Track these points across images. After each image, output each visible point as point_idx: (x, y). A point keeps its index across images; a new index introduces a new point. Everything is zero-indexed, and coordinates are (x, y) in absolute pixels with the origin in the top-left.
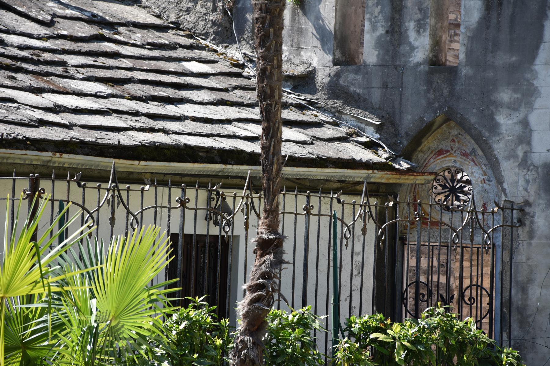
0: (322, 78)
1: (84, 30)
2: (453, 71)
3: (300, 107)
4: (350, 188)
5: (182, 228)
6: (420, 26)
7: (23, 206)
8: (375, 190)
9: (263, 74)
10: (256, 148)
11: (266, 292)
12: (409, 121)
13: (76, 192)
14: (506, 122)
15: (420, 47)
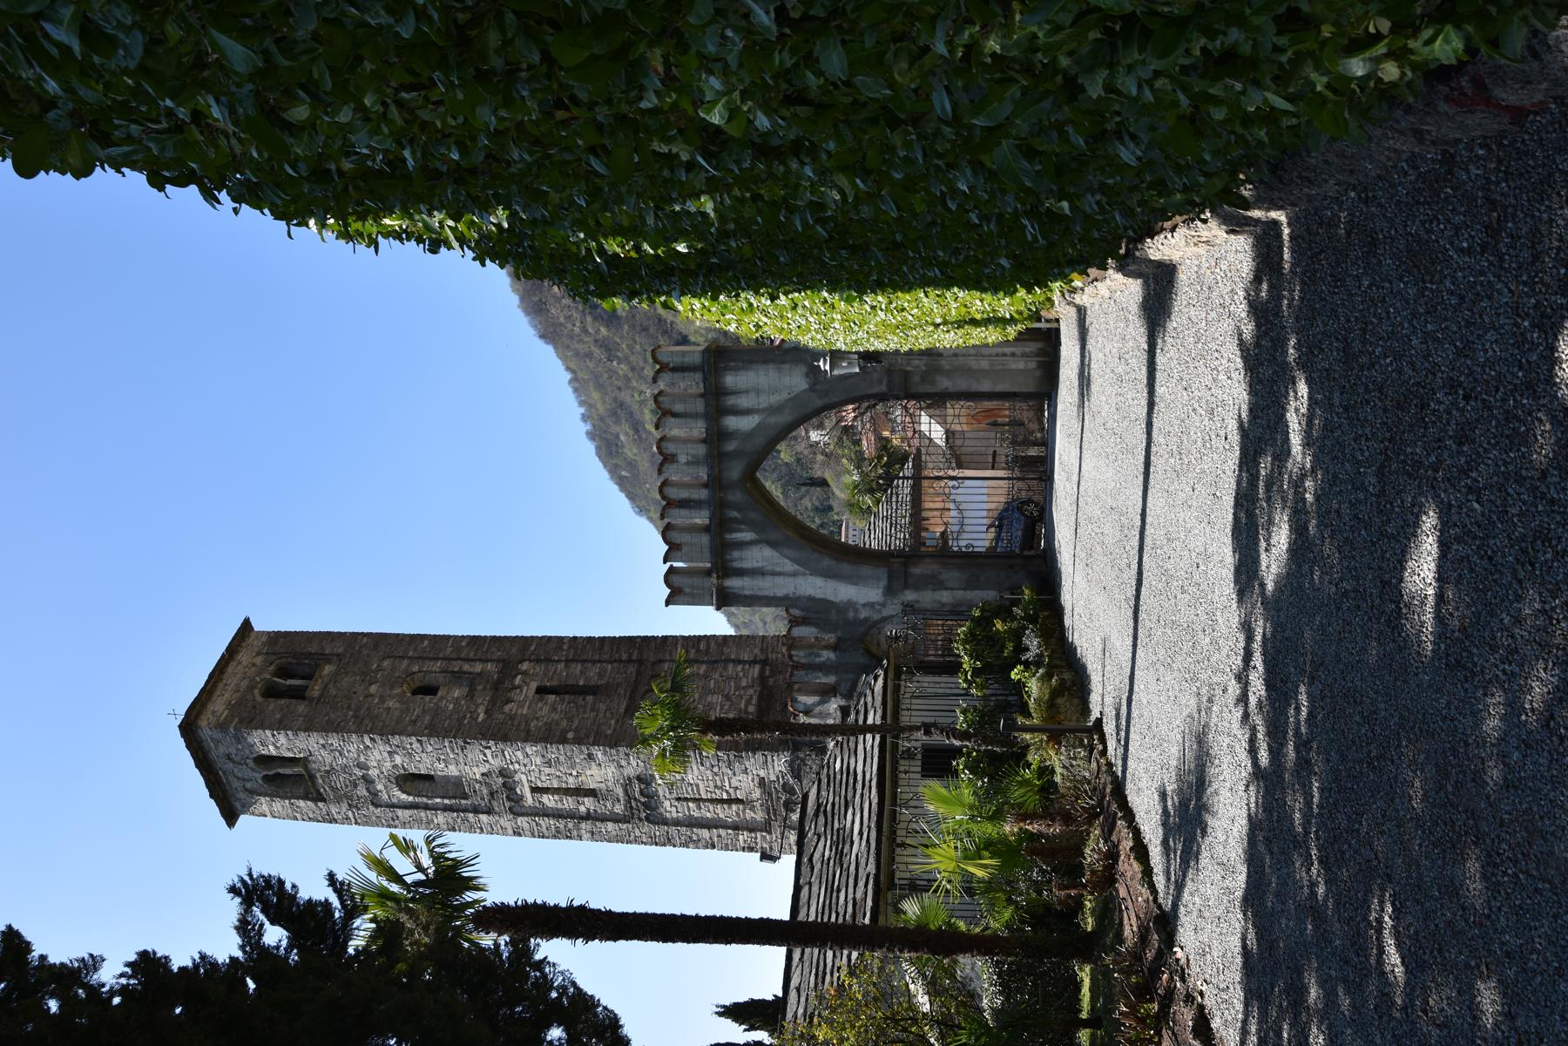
1: (821, 819)
2: (839, 639)
3: (857, 713)
4: (897, 689)
5: (803, 953)
6: (818, 655)
7: (910, 851)
8: (898, 676)
10: (878, 737)
11: (951, 731)
12: (862, 660)
13: (903, 825)
14: (863, 614)
15: (827, 655)
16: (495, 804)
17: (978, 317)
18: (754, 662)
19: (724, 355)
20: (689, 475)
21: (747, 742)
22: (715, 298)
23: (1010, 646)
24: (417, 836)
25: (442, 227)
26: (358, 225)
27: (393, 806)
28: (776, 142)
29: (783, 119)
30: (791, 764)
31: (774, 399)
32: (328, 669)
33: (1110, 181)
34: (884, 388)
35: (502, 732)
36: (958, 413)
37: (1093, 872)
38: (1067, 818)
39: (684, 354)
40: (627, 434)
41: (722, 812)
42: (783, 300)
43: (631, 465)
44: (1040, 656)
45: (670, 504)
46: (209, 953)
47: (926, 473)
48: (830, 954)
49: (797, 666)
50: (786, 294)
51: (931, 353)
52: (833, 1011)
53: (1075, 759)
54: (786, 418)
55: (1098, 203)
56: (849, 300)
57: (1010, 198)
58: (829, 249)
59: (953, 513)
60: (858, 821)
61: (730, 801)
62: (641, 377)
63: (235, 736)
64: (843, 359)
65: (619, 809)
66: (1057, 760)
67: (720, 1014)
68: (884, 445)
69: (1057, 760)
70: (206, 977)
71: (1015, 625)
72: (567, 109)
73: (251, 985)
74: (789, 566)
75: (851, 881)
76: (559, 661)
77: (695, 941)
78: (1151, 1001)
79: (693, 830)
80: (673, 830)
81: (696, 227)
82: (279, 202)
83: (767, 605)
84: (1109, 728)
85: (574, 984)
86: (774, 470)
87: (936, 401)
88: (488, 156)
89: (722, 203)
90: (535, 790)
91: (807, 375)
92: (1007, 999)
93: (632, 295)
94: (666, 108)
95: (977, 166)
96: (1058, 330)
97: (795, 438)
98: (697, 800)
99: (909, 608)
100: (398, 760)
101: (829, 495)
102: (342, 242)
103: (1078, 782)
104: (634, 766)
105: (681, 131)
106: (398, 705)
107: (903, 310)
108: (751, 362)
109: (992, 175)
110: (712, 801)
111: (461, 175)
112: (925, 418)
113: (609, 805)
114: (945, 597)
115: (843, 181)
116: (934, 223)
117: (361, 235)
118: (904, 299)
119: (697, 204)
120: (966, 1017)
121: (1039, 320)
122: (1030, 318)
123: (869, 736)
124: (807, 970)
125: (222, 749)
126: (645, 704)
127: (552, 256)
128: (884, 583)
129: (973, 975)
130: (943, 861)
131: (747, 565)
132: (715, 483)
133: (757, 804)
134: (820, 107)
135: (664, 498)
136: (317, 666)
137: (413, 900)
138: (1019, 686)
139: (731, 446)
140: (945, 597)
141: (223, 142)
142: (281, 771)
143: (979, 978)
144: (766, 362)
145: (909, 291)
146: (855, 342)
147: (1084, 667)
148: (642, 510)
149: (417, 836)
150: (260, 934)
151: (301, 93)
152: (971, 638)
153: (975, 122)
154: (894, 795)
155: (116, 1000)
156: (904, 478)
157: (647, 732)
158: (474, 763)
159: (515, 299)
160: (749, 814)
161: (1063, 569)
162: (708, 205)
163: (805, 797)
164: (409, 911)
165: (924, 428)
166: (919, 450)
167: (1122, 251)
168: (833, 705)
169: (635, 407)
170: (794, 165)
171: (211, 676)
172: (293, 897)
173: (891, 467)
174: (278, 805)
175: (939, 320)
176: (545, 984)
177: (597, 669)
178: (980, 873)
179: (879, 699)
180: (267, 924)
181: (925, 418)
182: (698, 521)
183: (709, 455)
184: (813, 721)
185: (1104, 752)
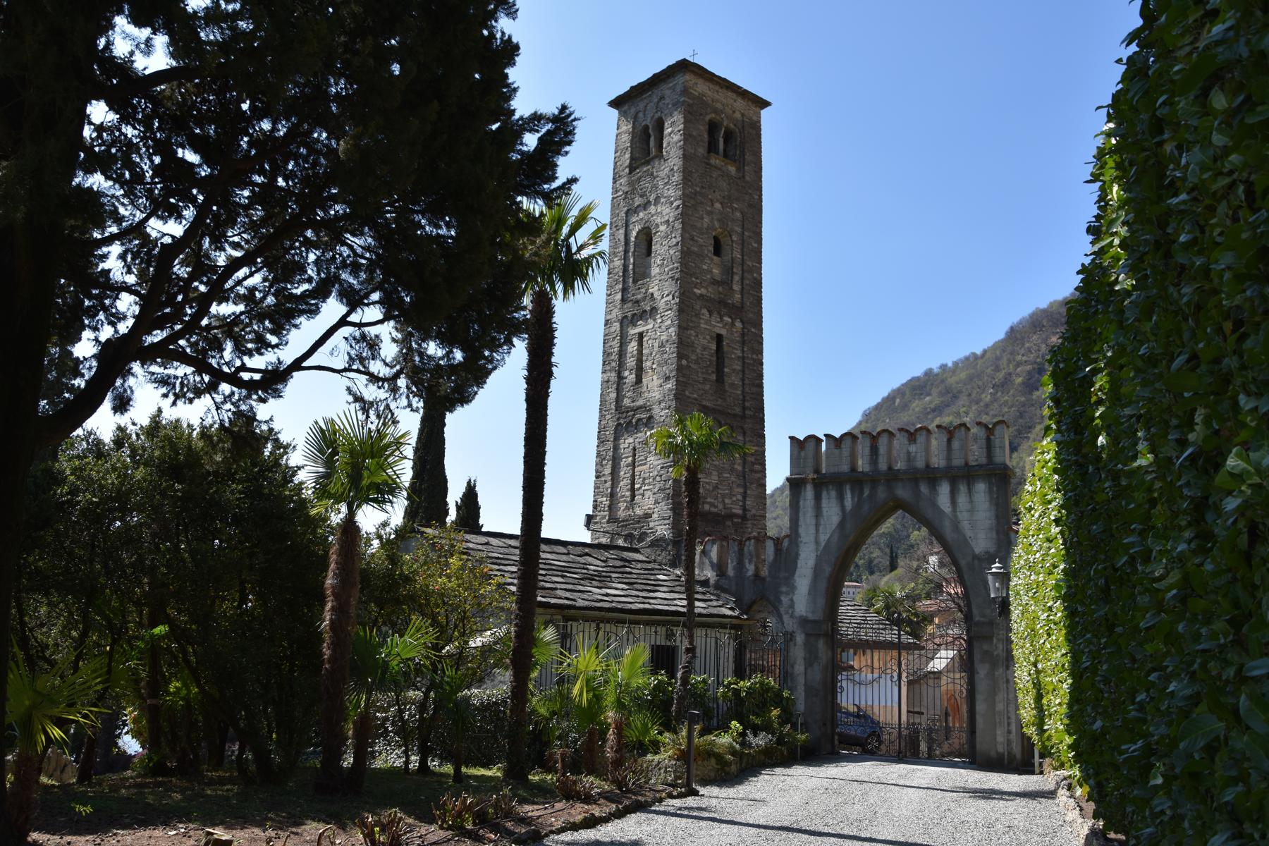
0: (712, 582)
1: (618, 563)
2: (764, 579)
4: (724, 626)
7: (593, 634)
8: (734, 627)
9: (687, 581)
10: (684, 610)
11: (688, 670)
13: (614, 629)
14: (784, 599)
15: (750, 569)
16: (630, 305)
17: (1044, 701)
18: (745, 509)
19: (1003, 482)
20: (898, 454)
21: (681, 504)
22: (1055, 471)
23: (758, 721)
24: (604, 245)
25: (1113, 234)
26: (1111, 164)
27: (627, 226)
28: (1209, 517)
29: (1235, 522)
30: (663, 539)
31: (965, 525)
32: (732, 169)
33: (1186, 825)
34: (977, 619)
35: (686, 309)
36: (956, 684)
37: (575, 782)
38: (618, 763)
39: (1002, 448)
40: (931, 402)
41: (624, 483)
42: (1055, 530)
43: (905, 407)
44: (750, 747)
45: (874, 439)
46: (518, 94)
47: (904, 654)
48: (514, 569)
49: (741, 544)
50: (1061, 532)
51: (1009, 660)
52: (471, 570)
53: (666, 772)
54: (949, 534)
55: (1163, 812)
56: (1057, 587)
57: (1163, 729)
58: (1105, 568)
59: (870, 676)
60: (616, 593)
61: (633, 490)
62: (980, 413)
63: (678, 102)
64: (1002, 584)
65: (627, 402)
66: (665, 757)
67: (469, 483)
68: (928, 618)
69: (665, 757)
70: (501, 91)
71: (776, 725)
72: (1234, 332)
73: (494, 127)
74: (824, 538)
75: (570, 587)
76: (743, 352)
77: (526, 463)
78: (474, 824)
79: (610, 461)
80: (610, 445)
81: (1123, 449)
82: (1130, 95)
83: (791, 520)
84: (691, 801)
85: (495, 368)
86: (903, 525)
87: (966, 663)
88: (1183, 267)
89: (1147, 472)
90: (641, 335)
91: (987, 553)
92: (477, 709)
93: (1057, 401)
94: (1240, 417)
95: (1195, 700)
96: (1032, 773)
97: (931, 543)
98: (633, 464)
99: (789, 637)
100: (663, 228)
101: (883, 572)
102: (1095, 152)
103: (646, 773)
104: (660, 413)
105: (1217, 433)
106: (705, 225)
107: (1049, 635)
108: (997, 505)
109: (1185, 714)
110: (633, 476)
111: (1164, 247)
112: (951, 654)
113: (630, 394)
114: (799, 668)
115: (1175, 577)
116: (1134, 660)
117: (1102, 167)
118: (1060, 636)
119: (1145, 451)
120: (466, 675)
121: (1042, 756)
122: (1044, 747)
123: (685, 603)
124: (502, 550)
125: (668, 92)
126: (710, 421)
127: (1088, 330)
128: (811, 617)
129: (496, 682)
130: (586, 660)
131: (824, 503)
132: (892, 476)
133: (630, 512)
134: (1248, 557)
135: (879, 433)
136: (735, 161)
137: (557, 244)
138: (725, 728)
139: (924, 489)
140: (799, 668)
141: (1188, 39)
142: (652, 139)
143: (494, 687)
144: (997, 517)
145: (1067, 639)
146: (1018, 594)
147: (740, 783)
148: (867, 416)
149: (604, 245)
150: (531, 131)
151: (1241, 98)
152: (765, 688)
153: (1243, 697)
154: (638, 623)
155: (485, 32)
156: (899, 635)
157: (688, 423)
158: (661, 287)
159: (1044, 305)
160: (623, 505)
161: (823, 768)
162: (1145, 460)
163: (636, 551)
164: (548, 241)
165: (943, 653)
166: (923, 648)
167: (1112, 835)
168: (709, 574)
169: (954, 409)
170: (1187, 534)
171: (725, 80)
172: (558, 153)
173: (909, 625)
174: (626, 138)
175: (1040, 666)
176: (495, 346)
177: (738, 382)
178: (576, 690)
179: (715, 611)
180: (539, 135)
181: (951, 654)
182: (860, 463)
183: (916, 470)
184: (697, 557)
185: (671, 796)
